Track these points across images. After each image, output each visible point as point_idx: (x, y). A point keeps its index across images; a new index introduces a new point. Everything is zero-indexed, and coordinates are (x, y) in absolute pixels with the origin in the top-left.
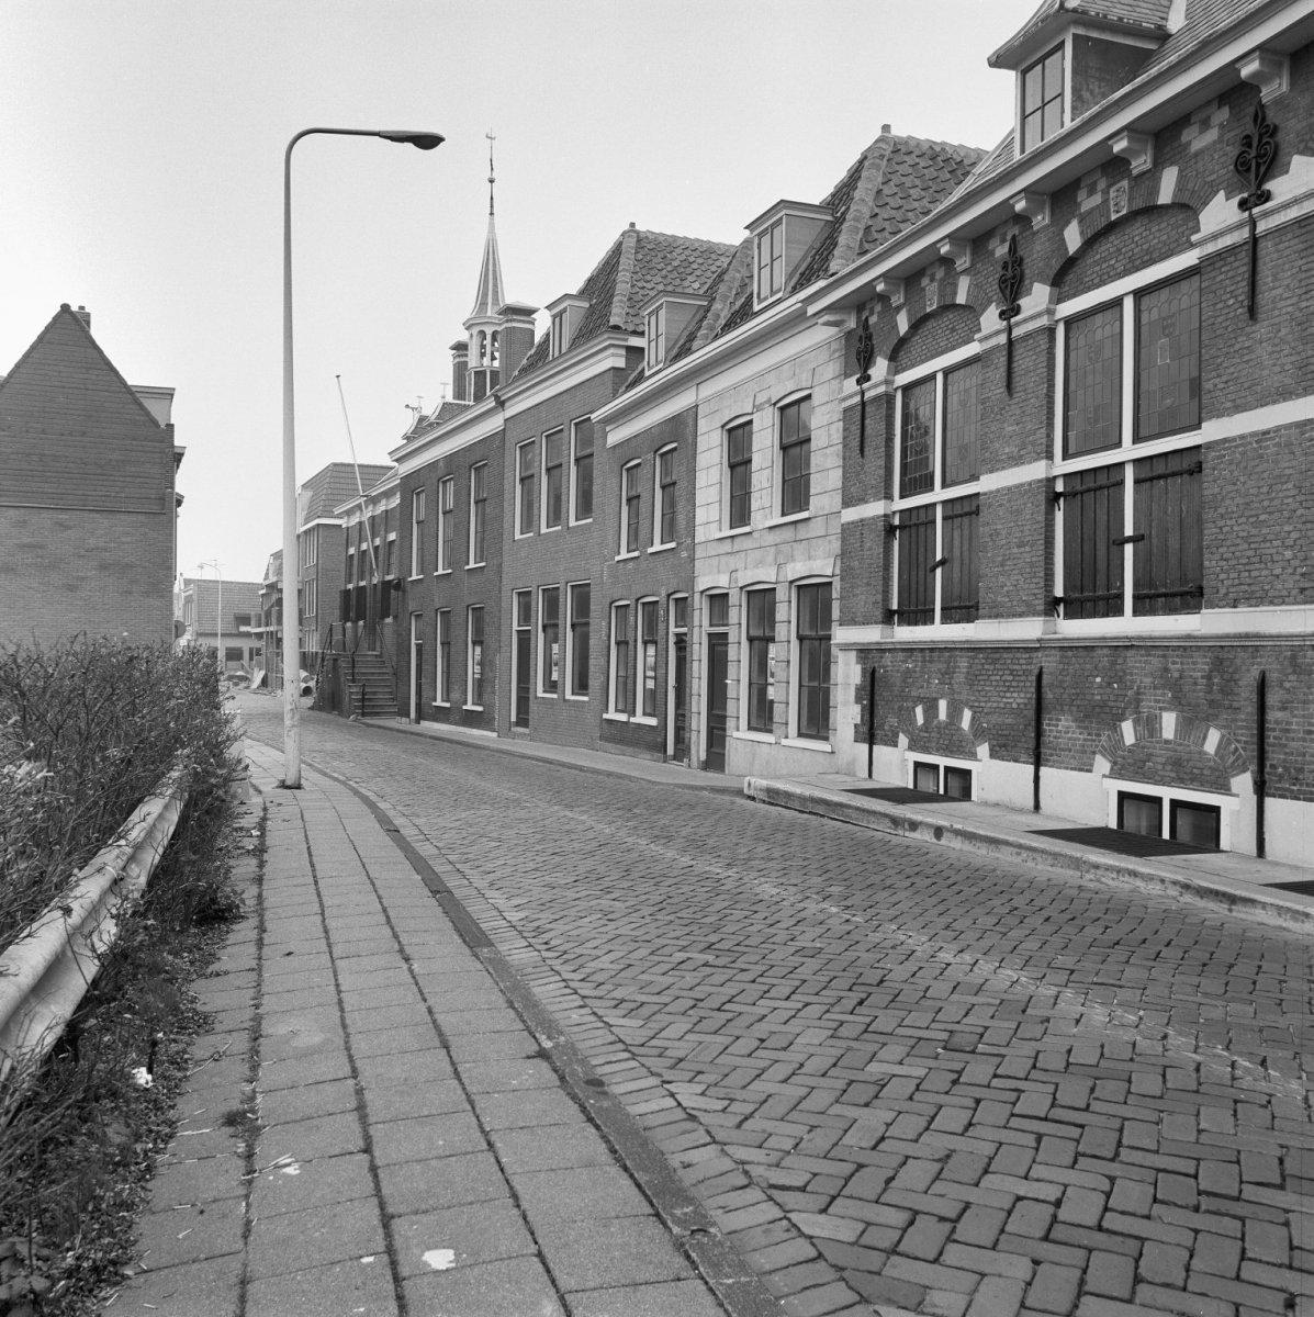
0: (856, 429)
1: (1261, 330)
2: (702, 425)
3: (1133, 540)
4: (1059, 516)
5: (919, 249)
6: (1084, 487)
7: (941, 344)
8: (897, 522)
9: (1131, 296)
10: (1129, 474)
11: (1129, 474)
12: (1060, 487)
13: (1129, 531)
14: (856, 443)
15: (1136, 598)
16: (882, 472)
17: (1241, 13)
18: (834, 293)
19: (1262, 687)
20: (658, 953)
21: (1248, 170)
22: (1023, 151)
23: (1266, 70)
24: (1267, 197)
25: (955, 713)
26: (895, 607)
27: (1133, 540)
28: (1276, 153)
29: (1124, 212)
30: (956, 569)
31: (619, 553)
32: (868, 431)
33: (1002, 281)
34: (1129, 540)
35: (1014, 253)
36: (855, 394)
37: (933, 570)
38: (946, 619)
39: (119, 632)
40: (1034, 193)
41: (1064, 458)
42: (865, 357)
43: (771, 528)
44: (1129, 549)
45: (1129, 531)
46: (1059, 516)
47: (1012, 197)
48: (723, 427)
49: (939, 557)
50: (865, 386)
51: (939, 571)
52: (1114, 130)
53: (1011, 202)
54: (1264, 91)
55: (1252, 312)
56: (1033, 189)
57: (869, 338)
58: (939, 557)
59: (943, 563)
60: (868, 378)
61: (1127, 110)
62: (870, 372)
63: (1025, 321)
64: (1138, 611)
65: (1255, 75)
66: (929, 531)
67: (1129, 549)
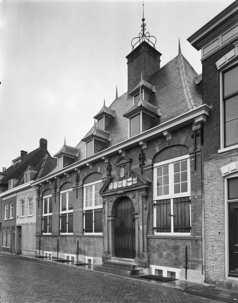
0: (38, 204)
1: (78, 200)
2: (17, 199)
3: (68, 223)
4: (84, 217)
5: (93, 160)
6: (167, 202)
7: (176, 153)
8: (43, 218)
9: (173, 164)
10: (172, 201)
11: (172, 201)
12: (84, 212)
13: (67, 222)
14: (38, 206)
15: (68, 231)
16: (41, 211)
17: (90, 156)
18: (115, 149)
19: (78, 242)
20: (31, 301)
21: (141, 160)
22: (130, 137)
23: (122, 152)
24: (144, 164)
25: (49, 245)
26: (43, 230)
27: (68, 223)
28: (145, 158)
29: (93, 172)
30: (50, 225)
31: (4, 219)
32: (40, 205)
33: (76, 180)
34: (67, 223)
35: (142, 152)
36: (38, 199)
37: (67, 224)
38: (49, 232)
39: (151, 274)
40: (78, 168)
41: (158, 195)
42: (109, 170)
43: (27, 217)
44: (67, 224)
45: (67, 222)
46: (84, 217)
47: (87, 163)
48: (20, 200)
49: (48, 223)
50: (196, 151)
51: (48, 225)
52: (197, 116)
53: (139, 142)
54: (167, 138)
55: (77, 197)
56: (168, 130)
57: (40, 191)
58: (48, 223)
59: (48, 224)
60: (78, 184)
61: (119, 147)
62: (79, 183)
63: (79, 186)
64: (175, 231)
65: (142, 145)
66: (168, 206)
67: (67, 224)
